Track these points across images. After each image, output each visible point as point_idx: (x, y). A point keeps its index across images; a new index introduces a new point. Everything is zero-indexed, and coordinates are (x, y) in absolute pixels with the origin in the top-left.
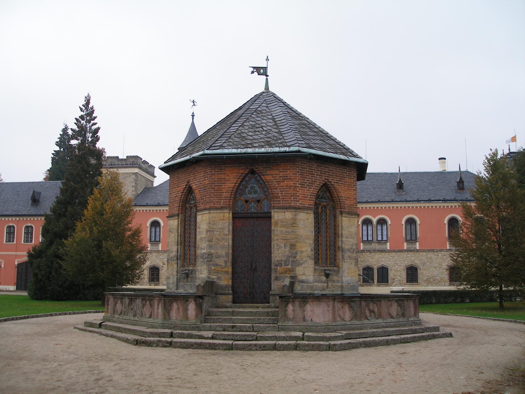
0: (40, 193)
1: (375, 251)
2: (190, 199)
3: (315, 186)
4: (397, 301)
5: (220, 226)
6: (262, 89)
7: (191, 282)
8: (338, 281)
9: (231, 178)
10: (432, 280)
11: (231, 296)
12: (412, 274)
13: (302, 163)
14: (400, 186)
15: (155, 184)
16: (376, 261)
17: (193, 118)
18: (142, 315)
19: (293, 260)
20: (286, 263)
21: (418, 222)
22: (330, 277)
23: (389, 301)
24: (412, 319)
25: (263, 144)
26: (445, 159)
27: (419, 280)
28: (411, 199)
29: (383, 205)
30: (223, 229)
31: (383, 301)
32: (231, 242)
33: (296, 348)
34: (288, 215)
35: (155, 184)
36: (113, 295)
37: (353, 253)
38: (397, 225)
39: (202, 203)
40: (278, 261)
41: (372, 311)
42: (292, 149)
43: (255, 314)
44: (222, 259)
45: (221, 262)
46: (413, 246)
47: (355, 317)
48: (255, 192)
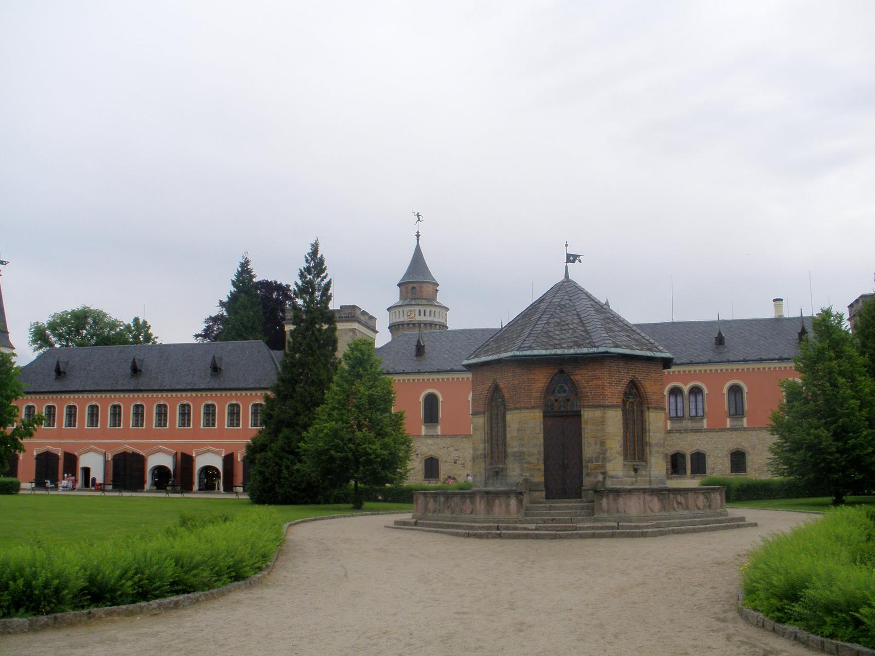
0: (221, 359)
1: (686, 431)
4: (703, 494)
6: (562, 278)
8: (646, 476)
12: (738, 460)
14: (720, 341)
15: (378, 345)
16: (687, 445)
17: (418, 240)
18: (461, 511)
19: (603, 457)
21: (746, 390)
24: (719, 510)
25: (571, 344)
26: (781, 300)
27: (748, 469)
28: (735, 359)
29: (697, 368)
32: (542, 440)
33: (613, 535)
34: (598, 413)
35: (378, 345)
36: (424, 494)
38: (717, 397)
41: (679, 503)
42: (601, 350)
43: (571, 508)
45: (533, 459)
46: (740, 423)
47: (664, 508)
48: (565, 391)
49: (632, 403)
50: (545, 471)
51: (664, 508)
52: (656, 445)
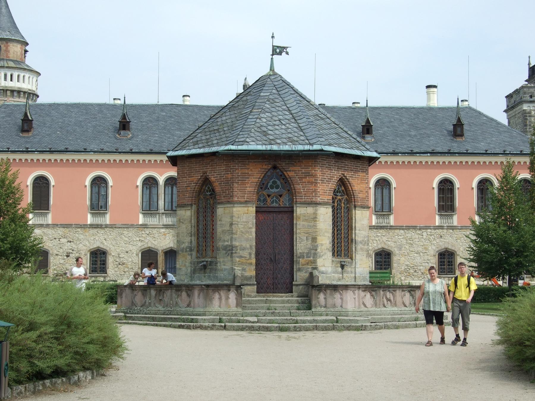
2: (204, 190)
3: (333, 182)
4: (409, 291)
5: (244, 220)
7: (210, 273)
9: (254, 174)
10: (412, 271)
11: (256, 286)
12: (98, 259)
13: (322, 160)
20: (308, 255)
22: (345, 268)
23: (403, 291)
25: (285, 140)
30: (247, 222)
31: (398, 291)
32: (254, 235)
34: (310, 210)
37: (364, 245)
39: (224, 197)
40: (300, 253)
44: (246, 251)
45: (245, 254)
47: (376, 305)
48: (277, 187)
49: (340, 200)
50: (257, 264)
51: (376, 305)
52: (361, 242)
